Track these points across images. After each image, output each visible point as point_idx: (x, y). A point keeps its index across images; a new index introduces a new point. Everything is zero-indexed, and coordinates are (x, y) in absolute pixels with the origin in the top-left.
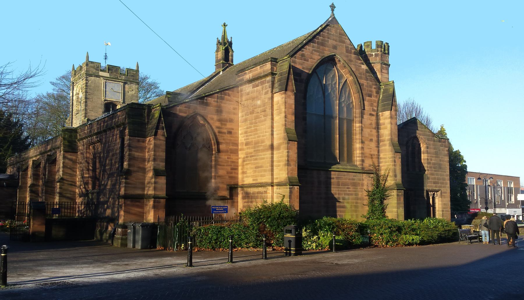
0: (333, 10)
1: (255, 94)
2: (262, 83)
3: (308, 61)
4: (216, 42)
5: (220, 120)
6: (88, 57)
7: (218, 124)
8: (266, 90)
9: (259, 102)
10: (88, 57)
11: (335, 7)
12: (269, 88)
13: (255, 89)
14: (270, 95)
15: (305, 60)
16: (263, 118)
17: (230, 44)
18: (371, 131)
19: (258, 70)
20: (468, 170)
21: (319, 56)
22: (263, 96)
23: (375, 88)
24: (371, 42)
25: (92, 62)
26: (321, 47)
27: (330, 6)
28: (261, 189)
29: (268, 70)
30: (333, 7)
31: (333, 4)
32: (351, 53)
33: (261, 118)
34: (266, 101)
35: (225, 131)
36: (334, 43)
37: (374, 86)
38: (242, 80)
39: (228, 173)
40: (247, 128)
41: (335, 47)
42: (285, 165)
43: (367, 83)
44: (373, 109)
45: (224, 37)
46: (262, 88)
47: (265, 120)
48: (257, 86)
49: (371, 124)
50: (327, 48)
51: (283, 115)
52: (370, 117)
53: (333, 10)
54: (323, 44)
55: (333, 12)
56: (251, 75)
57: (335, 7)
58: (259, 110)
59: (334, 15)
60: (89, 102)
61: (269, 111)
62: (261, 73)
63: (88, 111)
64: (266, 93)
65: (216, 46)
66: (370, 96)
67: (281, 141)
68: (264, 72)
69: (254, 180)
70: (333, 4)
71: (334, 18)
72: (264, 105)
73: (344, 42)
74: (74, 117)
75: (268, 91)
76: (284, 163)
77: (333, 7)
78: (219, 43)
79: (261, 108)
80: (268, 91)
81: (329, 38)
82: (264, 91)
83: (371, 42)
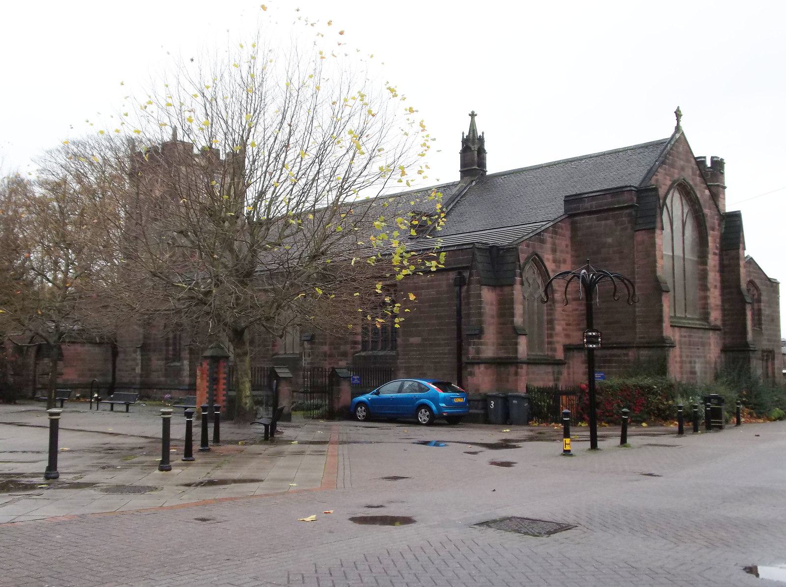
5: (555, 261)
13: (603, 222)
36: (682, 163)
39: (564, 329)
41: (683, 169)
48: (606, 219)
54: (672, 166)
66: (713, 229)
79: (615, 249)
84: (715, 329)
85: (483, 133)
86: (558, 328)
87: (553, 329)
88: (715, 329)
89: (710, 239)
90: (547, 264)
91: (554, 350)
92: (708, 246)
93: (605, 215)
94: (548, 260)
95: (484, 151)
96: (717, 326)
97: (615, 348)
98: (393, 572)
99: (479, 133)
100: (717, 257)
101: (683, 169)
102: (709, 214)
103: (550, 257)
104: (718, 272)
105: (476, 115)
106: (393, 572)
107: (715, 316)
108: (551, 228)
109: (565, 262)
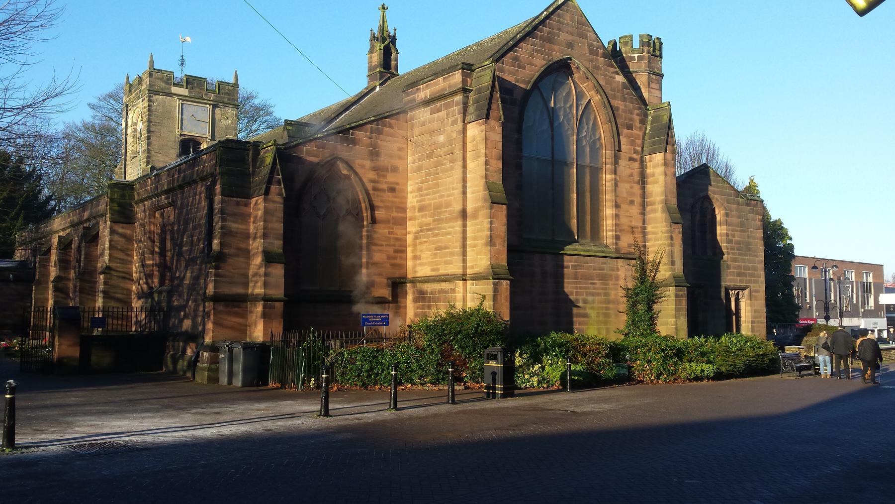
1: (435, 125)
2: (447, 106)
3: (524, 68)
5: (376, 169)
6: (152, 62)
7: (372, 175)
8: (453, 118)
9: (442, 138)
10: (152, 62)
13: (436, 115)
14: (460, 126)
15: (519, 67)
16: (448, 165)
17: (393, 39)
18: (632, 187)
19: (440, 84)
22: (449, 128)
23: (638, 115)
24: (631, 36)
25: (159, 71)
26: (547, 45)
28: (445, 286)
32: (597, 55)
34: (454, 135)
35: (385, 186)
36: (569, 38)
37: (636, 111)
38: (414, 100)
39: (389, 258)
40: (422, 182)
41: (570, 45)
42: (486, 244)
43: (625, 106)
46: (447, 114)
47: (452, 169)
48: (439, 111)
49: (631, 175)
50: (556, 47)
52: (629, 163)
54: (549, 40)
56: (428, 92)
58: (442, 151)
61: (458, 153)
62: (444, 89)
64: (454, 123)
68: (450, 86)
69: (433, 270)
72: (450, 142)
73: (585, 37)
74: (128, 163)
75: (457, 119)
76: (483, 241)
79: (446, 149)
80: (457, 119)
81: (559, 30)
83: (631, 36)
102: (622, 107)
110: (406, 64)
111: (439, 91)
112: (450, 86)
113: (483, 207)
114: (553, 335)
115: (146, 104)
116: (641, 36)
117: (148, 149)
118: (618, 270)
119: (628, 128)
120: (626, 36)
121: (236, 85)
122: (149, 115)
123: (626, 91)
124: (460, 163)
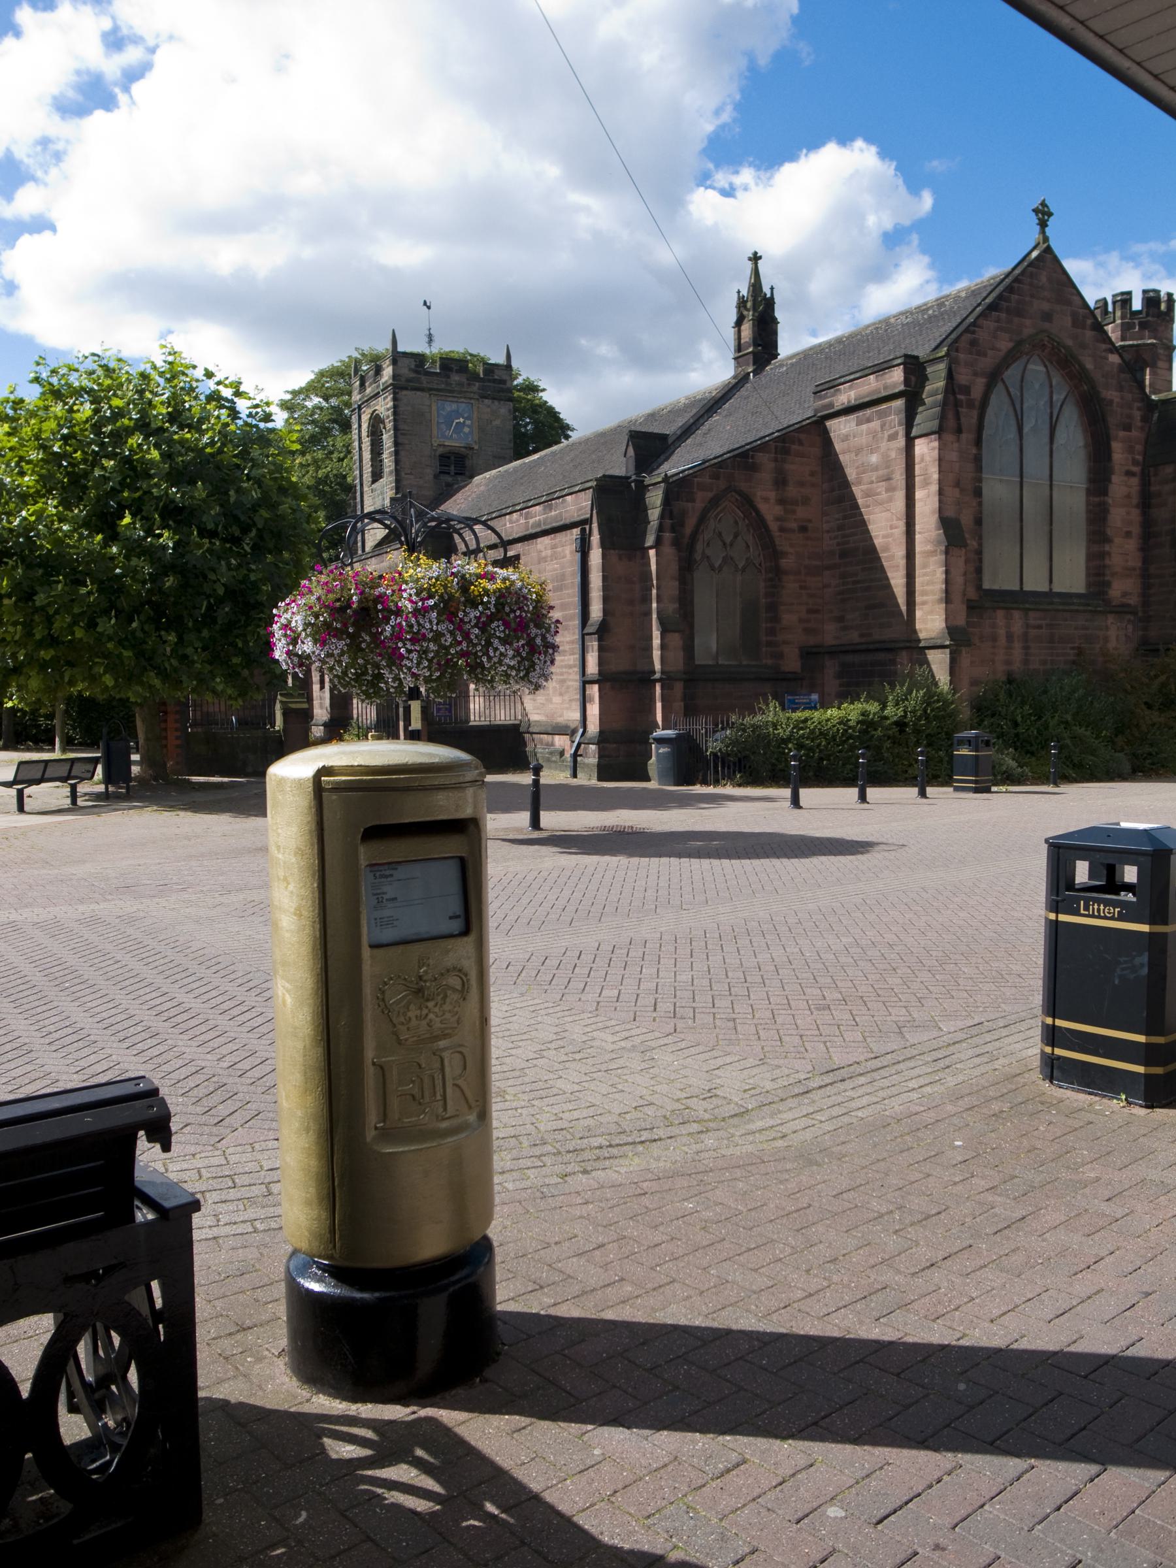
0: (1043, 224)
1: (863, 440)
2: (881, 415)
3: (985, 355)
4: (734, 301)
5: (781, 501)
6: (394, 342)
7: (778, 510)
8: (892, 431)
9: (874, 459)
10: (394, 342)
11: (1050, 214)
12: (900, 425)
13: (864, 427)
14: (901, 442)
15: (979, 353)
16: (884, 496)
17: (770, 303)
18: (1128, 513)
19: (871, 386)
20: (509, 1295)
21: (1011, 340)
22: (884, 445)
23: (1139, 409)
24: (1130, 293)
25: (405, 354)
26: (1016, 320)
27: (1036, 211)
28: (881, 656)
29: (895, 385)
30: (1043, 214)
31: (1043, 204)
32: (1084, 327)
33: (878, 494)
34: (893, 455)
35: (794, 525)
36: (1046, 306)
37: (1137, 405)
38: (831, 405)
39: (801, 620)
40: (845, 518)
41: (1047, 317)
42: (940, 601)
43: (1122, 398)
44: (1133, 459)
45: (756, 285)
46: (883, 426)
47: (890, 500)
48: (869, 420)
49: (1128, 496)
50: (1028, 322)
51: (934, 488)
52: (1125, 478)
53: (1043, 224)
54: (1019, 313)
55: (1043, 232)
56: (852, 394)
57: (1050, 214)
58: (874, 476)
59: (1046, 239)
60: (402, 453)
61: (899, 477)
62: (878, 391)
63: (403, 474)
64: (892, 437)
65: (735, 311)
66: (1127, 428)
67: (929, 547)
68: (885, 388)
69: (862, 636)
70: (1043, 204)
71: (1048, 250)
72: (887, 462)
73: (1069, 303)
74: (366, 489)
75: (896, 433)
76: (937, 597)
77: (1043, 214)
78: (742, 303)
79: (881, 472)
80: (896, 433)
81: (1032, 296)
82: (886, 434)
83: (1130, 293)
84: (1121, 610)
85: (772, 288)
86: (788, 618)
87: (776, 619)
88: (1121, 610)
89: (1116, 446)
90: (763, 507)
91: (780, 656)
92: (1110, 458)
93: (868, 412)
94: (766, 500)
95: (775, 321)
96: (1129, 605)
97: (877, 650)
98: (825, 980)
99: (766, 290)
100: (1135, 481)
101: (1047, 317)
102: (1116, 400)
103: (772, 495)
104: (1137, 506)
105: (760, 258)
106: (825, 980)
107: (1123, 588)
108: (773, 444)
109: (806, 501)
110: (788, 345)
111: (869, 395)
112: (885, 388)
113: (935, 551)
114: (278, 654)
115: (391, 404)
116: (1145, 292)
117: (396, 470)
118: (1107, 628)
119: (1124, 430)
120: (1122, 294)
121: (508, 367)
122: (395, 420)
123: (1122, 376)
124: (900, 495)
